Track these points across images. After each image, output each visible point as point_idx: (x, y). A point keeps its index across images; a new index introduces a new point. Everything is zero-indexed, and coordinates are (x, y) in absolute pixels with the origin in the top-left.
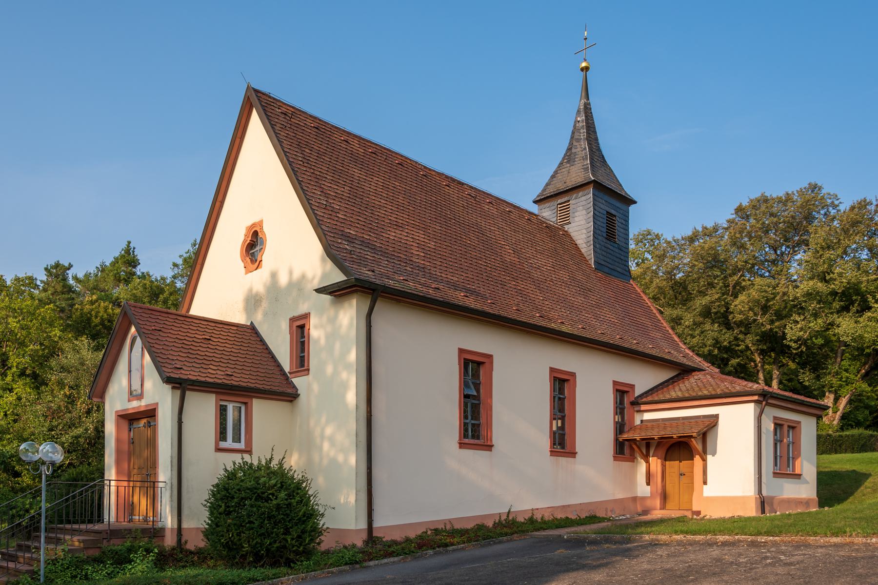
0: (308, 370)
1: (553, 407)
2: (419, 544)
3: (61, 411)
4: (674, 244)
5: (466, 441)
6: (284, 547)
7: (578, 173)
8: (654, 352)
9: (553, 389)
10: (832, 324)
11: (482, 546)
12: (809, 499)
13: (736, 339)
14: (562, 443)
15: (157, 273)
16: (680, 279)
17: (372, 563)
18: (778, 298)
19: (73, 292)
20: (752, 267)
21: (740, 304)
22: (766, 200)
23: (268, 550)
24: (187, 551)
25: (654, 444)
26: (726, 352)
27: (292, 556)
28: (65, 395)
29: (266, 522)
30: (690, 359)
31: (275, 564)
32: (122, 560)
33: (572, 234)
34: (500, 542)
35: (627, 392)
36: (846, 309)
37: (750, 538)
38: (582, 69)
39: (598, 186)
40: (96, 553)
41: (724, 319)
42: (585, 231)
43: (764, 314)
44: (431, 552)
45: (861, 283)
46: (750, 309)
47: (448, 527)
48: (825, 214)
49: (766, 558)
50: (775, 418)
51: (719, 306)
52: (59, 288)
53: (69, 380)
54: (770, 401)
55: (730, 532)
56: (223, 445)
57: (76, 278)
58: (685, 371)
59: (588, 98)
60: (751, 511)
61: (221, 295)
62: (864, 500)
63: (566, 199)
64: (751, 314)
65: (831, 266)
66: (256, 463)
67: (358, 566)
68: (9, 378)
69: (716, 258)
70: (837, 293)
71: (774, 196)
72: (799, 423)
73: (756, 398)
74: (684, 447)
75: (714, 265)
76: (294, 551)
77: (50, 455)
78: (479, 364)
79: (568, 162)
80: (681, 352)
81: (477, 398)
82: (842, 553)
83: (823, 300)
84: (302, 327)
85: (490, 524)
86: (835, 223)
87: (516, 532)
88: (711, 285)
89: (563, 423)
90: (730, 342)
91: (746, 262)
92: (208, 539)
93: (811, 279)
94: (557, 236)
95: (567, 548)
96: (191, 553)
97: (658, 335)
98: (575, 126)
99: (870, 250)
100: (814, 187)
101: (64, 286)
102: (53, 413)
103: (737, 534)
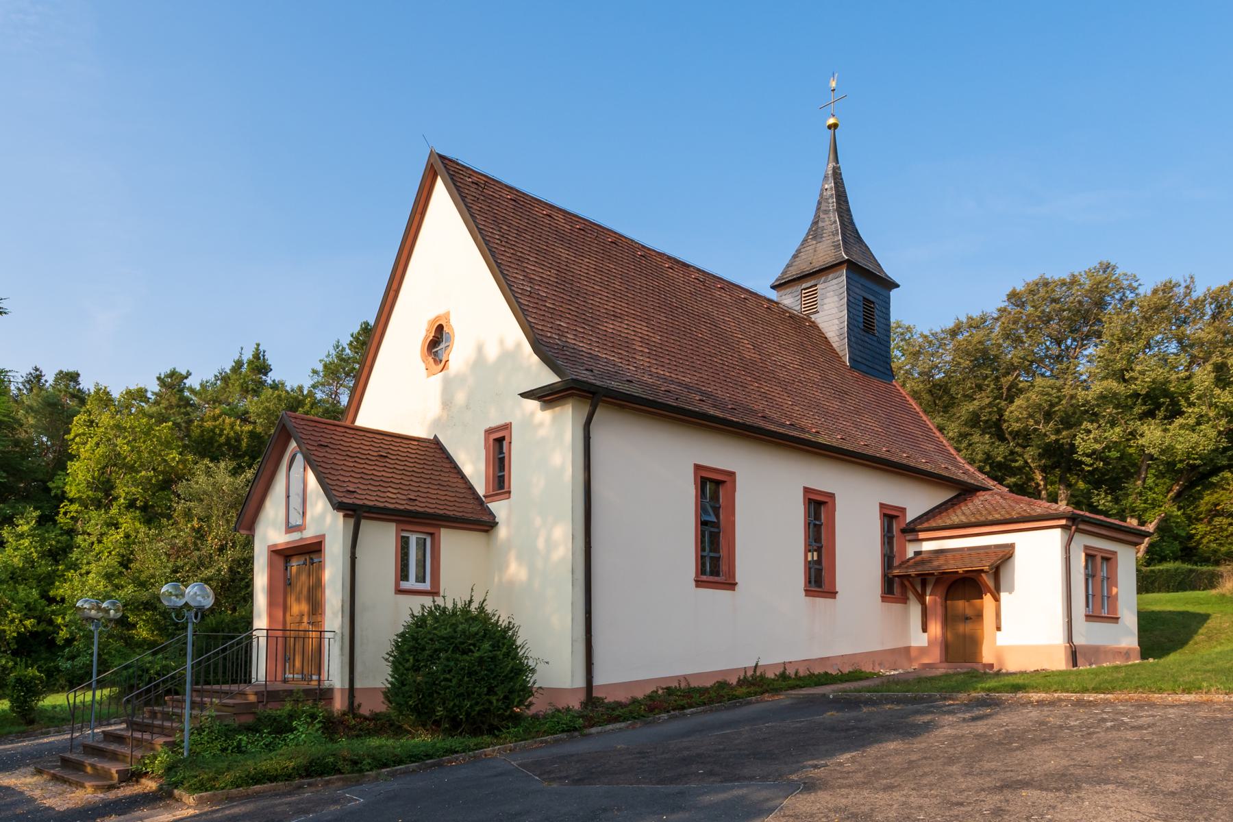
0: (509, 492)
1: (807, 536)
2: (649, 707)
3: (188, 548)
4: (931, 338)
5: (704, 578)
6: (487, 710)
7: (825, 252)
8: (929, 468)
9: (808, 514)
10: (1133, 434)
11: (727, 709)
12: (1129, 649)
13: (1012, 453)
14: (819, 580)
15: (291, 383)
16: (940, 380)
17: (593, 730)
18: (1064, 402)
19: (192, 405)
20: (1029, 365)
21: (1016, 411)
22: (1046, 284)
23: (468, 714)
24: (361, 716)
25: (932, 580)
26: (1000, 470)
27: (496, 722)
28: (193, 528)
29: (466, 679)
30: (972, 476)
31: (476, 732)
32: (281, 728)
33: (821, 326)
34: (749, 703)
35: (897, 517)
36: (1151, 414)
37: (1074, 697)
38: (829, 127)
39: (852, 266)
40: (248, 720)
41: (997, 429)
42: (837, 322)
43: (1047, 422)
44: (665, 716)
45: (1170, 382)
46: (1031, 416)
47: (683, 686)
48: (1121, 299)
49: (1104, 720)
50: (1086, 547)
51: (990, 413)
52: (174, 401)
53: (198, 510)
54: (1081, 526)
55: (1047, 689)
56: (405, 585)
57: (192, 391)
58: (966, 491)
59: (836, 160)
60: (1060, 663)
61: (398, 401)
62: (1201, 650)
63: (812, 283)
64: (1031, 422)
65: (1130, 362)
66: (450, 606)
67: (576, 734)
68: (114, 511)
69: (985, 352)
70: (1139, 395)
71: (1056, 278)
72: (1115, 553)
73: (1063, 522)
74: (965, 588)
75: (984, 363)
76: (499, 716)
77: (199, 598)
78: (718, 483)
79: (814, 238)
80: (960, 468)
81: (716, 525)
82: (1201, 714)
83: (1123, 405)
84: (500, 441)
85: (734, 681)
86: (1134, 309)
87: (767, 691)
88: (980, 388)
89: (819, 556)
90: (1005, 457)
91: (1024, 359)
92: (390, 702)
93: (1105, 378)
94: (804, 328)
95: (839, 710)
96: (366, 719)
97: (930, 447)
98: (821, 195)
99: (1180, 342)
100: (1106, 267)
101: (181, 399)
102: (178, 551)
103: (1056, 691)
